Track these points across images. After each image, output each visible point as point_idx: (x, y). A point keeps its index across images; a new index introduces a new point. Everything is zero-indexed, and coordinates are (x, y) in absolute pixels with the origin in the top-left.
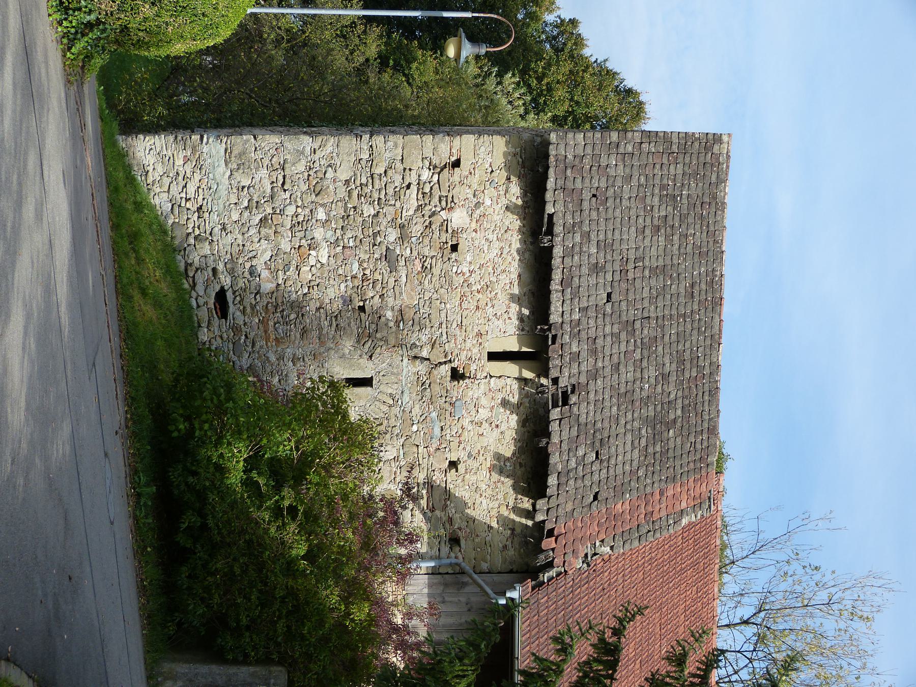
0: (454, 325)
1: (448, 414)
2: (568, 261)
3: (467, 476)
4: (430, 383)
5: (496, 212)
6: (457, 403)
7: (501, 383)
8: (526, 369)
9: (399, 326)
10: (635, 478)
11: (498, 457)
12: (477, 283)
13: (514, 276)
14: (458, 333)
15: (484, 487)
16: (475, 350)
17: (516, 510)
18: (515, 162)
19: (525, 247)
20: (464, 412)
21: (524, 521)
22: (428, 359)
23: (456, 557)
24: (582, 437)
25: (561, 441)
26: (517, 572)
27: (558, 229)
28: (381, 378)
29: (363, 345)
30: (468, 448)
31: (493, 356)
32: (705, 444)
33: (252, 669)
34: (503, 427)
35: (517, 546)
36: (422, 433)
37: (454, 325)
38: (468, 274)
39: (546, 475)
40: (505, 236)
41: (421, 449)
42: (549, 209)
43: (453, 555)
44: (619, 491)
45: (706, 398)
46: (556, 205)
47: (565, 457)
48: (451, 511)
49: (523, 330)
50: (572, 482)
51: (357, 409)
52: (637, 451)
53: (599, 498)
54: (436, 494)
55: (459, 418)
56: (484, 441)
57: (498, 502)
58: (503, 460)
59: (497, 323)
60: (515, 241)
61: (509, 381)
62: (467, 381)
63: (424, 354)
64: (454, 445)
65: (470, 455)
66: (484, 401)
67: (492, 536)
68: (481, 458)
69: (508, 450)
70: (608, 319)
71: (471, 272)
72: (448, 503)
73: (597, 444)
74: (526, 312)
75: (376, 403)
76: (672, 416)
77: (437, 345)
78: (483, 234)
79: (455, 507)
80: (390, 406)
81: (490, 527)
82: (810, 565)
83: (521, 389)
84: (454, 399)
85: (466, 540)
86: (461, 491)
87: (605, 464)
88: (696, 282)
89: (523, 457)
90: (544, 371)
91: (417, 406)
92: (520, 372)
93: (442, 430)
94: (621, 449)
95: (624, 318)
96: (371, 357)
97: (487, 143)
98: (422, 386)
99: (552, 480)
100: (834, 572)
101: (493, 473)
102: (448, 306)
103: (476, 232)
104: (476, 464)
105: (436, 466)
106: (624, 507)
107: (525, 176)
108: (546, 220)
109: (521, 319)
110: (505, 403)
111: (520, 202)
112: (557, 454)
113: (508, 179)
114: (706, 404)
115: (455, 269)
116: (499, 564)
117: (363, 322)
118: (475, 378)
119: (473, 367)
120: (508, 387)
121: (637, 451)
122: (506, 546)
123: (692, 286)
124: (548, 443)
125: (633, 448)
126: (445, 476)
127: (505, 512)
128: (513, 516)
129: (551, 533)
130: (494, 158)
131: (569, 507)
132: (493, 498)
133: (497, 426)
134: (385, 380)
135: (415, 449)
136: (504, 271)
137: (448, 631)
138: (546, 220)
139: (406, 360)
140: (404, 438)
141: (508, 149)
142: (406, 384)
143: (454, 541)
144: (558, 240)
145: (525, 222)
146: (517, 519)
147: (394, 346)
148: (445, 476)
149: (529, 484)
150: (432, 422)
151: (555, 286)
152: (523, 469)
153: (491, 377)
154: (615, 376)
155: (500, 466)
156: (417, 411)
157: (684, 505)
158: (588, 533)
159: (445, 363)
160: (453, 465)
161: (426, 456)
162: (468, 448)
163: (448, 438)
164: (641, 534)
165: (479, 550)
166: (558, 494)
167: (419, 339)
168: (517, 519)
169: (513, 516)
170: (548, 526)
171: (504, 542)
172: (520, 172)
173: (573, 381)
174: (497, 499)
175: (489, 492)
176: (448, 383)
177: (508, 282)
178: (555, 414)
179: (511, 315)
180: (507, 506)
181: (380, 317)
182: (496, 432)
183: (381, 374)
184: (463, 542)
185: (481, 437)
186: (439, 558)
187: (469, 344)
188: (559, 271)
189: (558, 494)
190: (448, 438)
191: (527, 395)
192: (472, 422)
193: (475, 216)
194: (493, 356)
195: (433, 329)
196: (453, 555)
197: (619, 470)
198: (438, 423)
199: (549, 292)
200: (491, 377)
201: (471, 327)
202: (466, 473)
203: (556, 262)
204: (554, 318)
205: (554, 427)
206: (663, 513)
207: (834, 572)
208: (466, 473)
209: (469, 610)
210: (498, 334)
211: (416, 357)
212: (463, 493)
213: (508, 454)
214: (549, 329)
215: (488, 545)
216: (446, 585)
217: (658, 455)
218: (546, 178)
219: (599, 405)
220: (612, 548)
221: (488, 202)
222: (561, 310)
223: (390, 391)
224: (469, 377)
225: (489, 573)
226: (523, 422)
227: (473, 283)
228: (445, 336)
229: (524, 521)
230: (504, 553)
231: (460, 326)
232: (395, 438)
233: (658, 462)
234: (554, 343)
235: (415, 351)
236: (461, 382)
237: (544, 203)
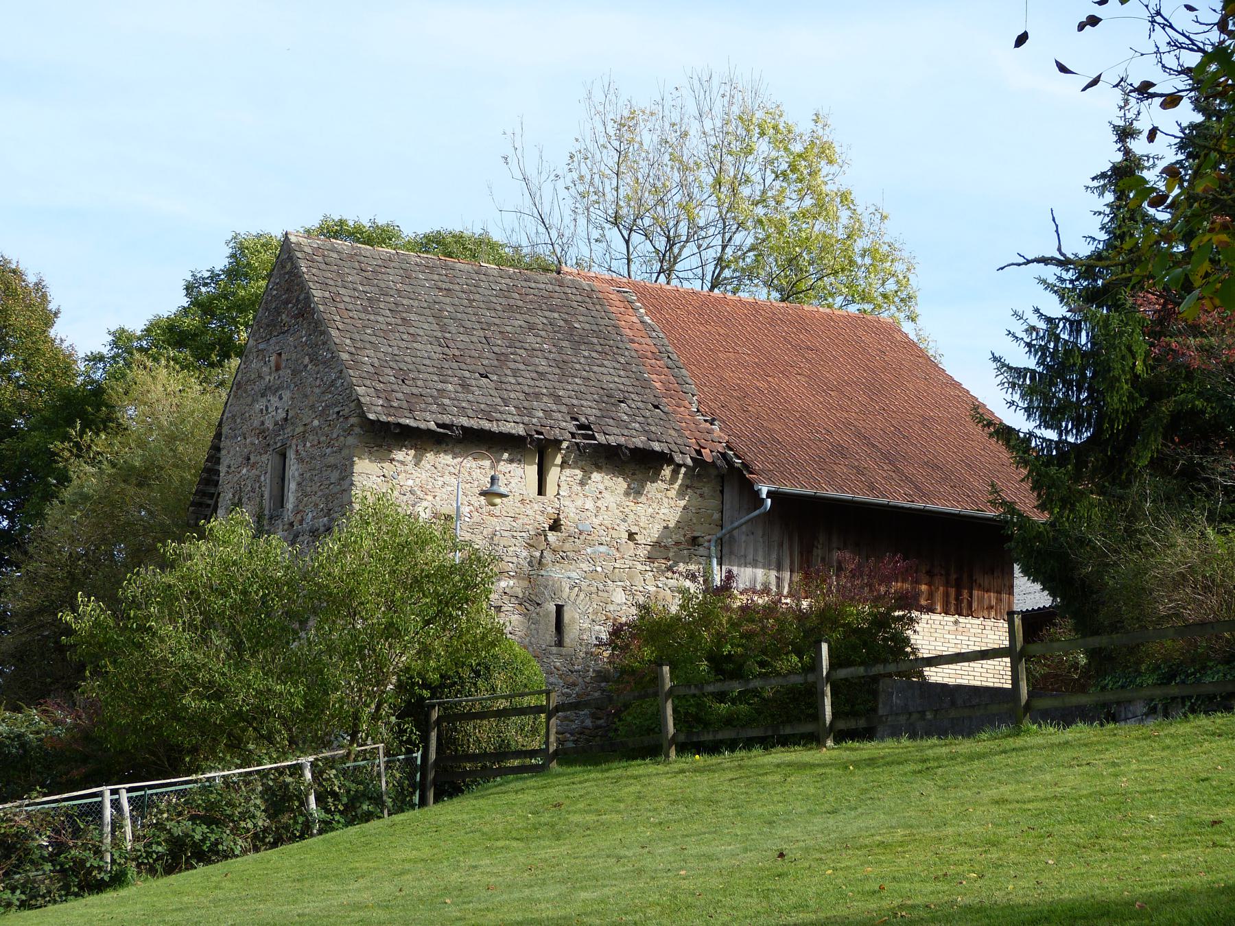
1: (588, 537)
2: (470, 413)
3: (641, 524)
7: (564, 486)
10: (628, 367)
11: (627, 494)
13: (474, 464)
15: (650, 510)
16: (536, 507)
21: (681, 476)
24: (613, 415)
26: (723, 486)
27: (446, 419)
31: (541, 491)
33: (880, 706)
34: (601, 487)
39: (653, 452)
40: (440, 469)
41: (617, 565)
42: (432, 426)
45: (533, 285)
47: (634, 433)
50: (653, 429)
54: (654, 555)
56: (613, 506)
59: (513, 485)
60: (446, 459)
61: (563, 478)
62: (561, 517)
63: (538, 554)
66: (579, 503)
69: (621, 484)
74: (506, 456)
76: (562, 323)
80: (580, 590)
81: (685, 508)
83: (570, 467)
86: (655, 532)
87: (627, 395)
90: (557, 443)
92: (556, 465)
94: (609, 378)
96: (538, 604)
99: (657, 447)
100: (577, 140)
101: (640, 500)
102: (498, 529)
104: (632, 516)
105: (631, 552)
107: (389, 446)
108: (442, 430)
109: (511, 461)
110: (582, 483)
111: (412, 452)
115: (467, 519)
116: (715, 503)
118: (559, 509)
119: (550, 510)
123: (440, 289)
124: (626, 447)
125: (602, 365)
127: (672, 493)
128: (676, 486)
129: (699, 452)
132: (660, 503)
135: (617, 570)
136: (470, 473)
137: (769, 555)
138: (442, 430)
139: (543, 572)
140: (607, 580)
146: (679, 482)
149: (651, 468)
151: (494, 427)
152: (637, 472)
153: (558, 494)
155: (635, 492)
156: (585, 566)
160: (631, 536)
161: (623, 561)
163: (608, 539)
167: (525, 558)
168: (679, 482)
169: (676, 486)
170: (694, 454)
175: (655, 505)
182: (606, 494)
184: (696, 534)
186: (709, 557)
187: (530, 512)
188: (482, 422)
190: (608, 539)
191: (575, 462)
192: (596, 516)
194: (541, 491)
196: (706, 544)
200: (558, 494)
203: (474, 423)
204: (520, 430)
205: (613, 440)
206: (648, 341)
211: (540, 563)
212: (655, 529)
216: (731, 553)
218: (408, 426)
219: (580, 395)
220: (693, 395)
221: (410, 482)
225: (722, 512)
226: (599, 468)
228: (523, 534)
229: (681, 476)
233: (608, 342)
234: (541, 434)
235: (535, 562)
237: (429, 431)
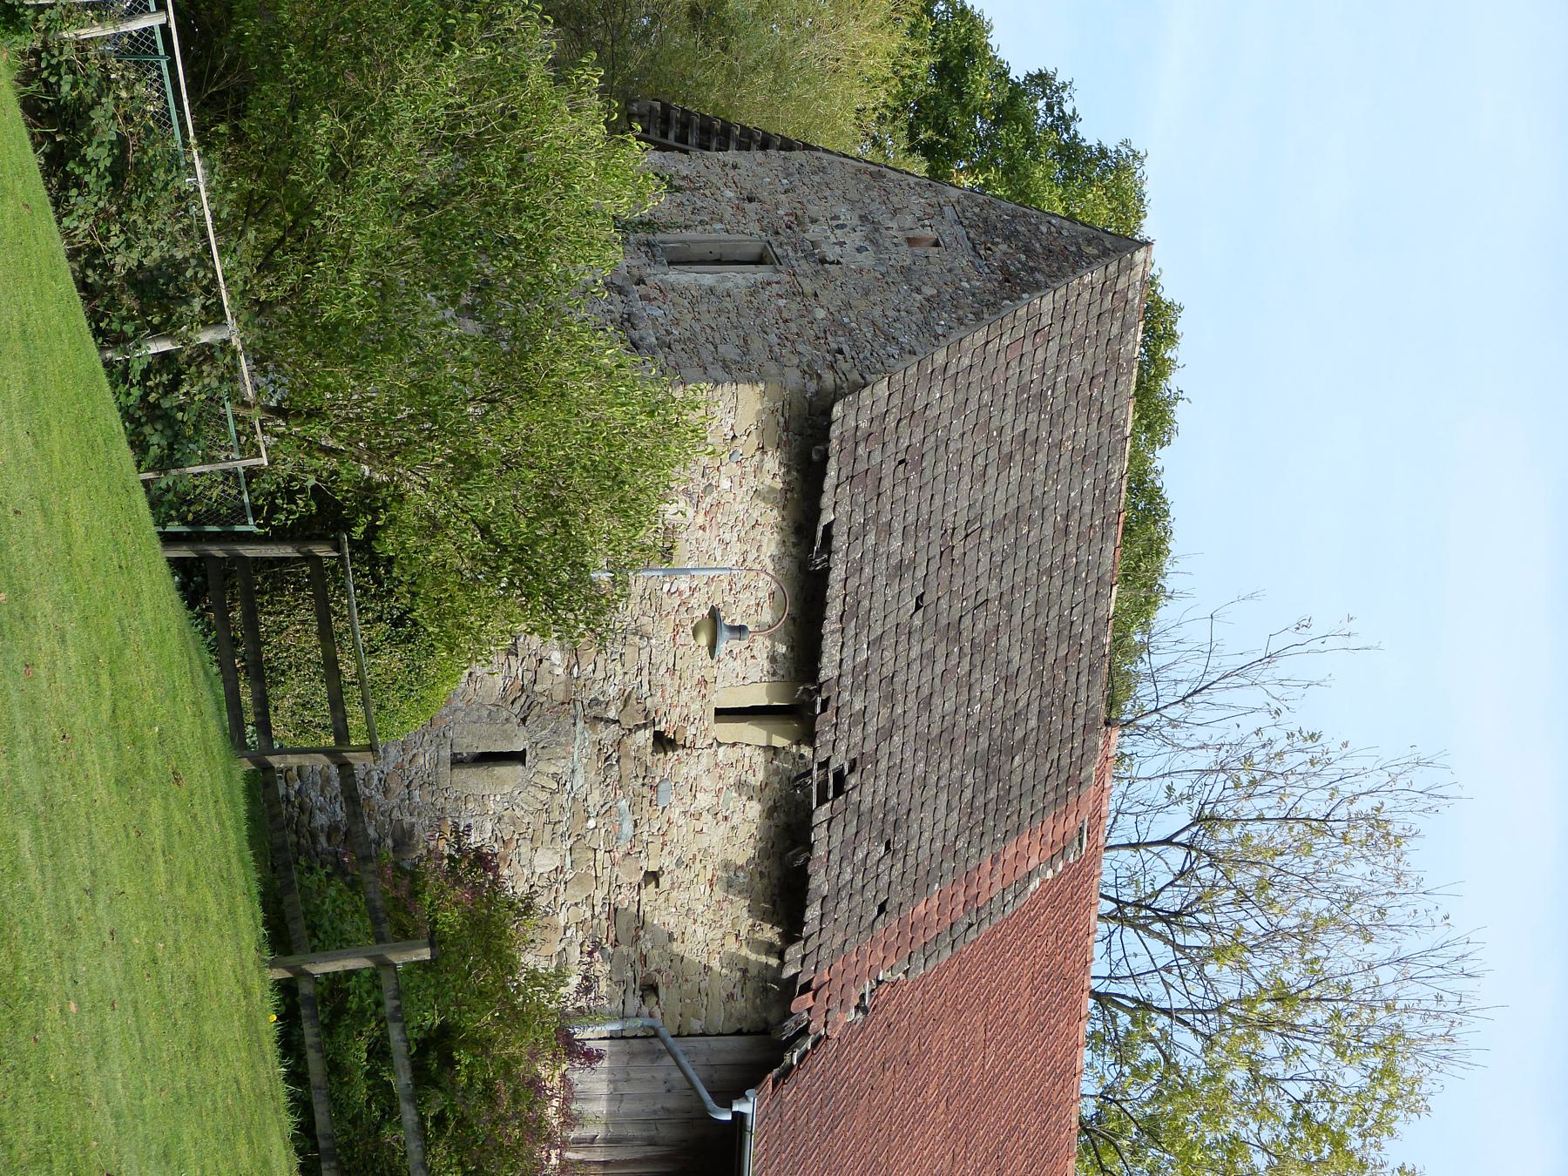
0: (663, 670)
1: (646, 802)
3: (674, 893)
4: (619, 758)
5: (738, 499)
6: (662, 787)
7: (734, 754)
8: (777, 734)
9: (571, 673)
12: (702, 607)
13: (763, 594)
14: (669, 682)
15: (700, 908)
16: (695, 706)
17: (750, 943)
18: (773, 423)
19: (783, 550)
20: (672, 798)
22: (618, 721)
23: (651, 1015)
24: (864, 833)
25: (829, 852)
26: (748, 1033)
27: (839, 542)
28: (539, 751)
29: (512, 703)
30: (677, 852)
31: (722, 714)
32: (1078, 752)
35: (751, 996)
36: (603, 831)
37: (663, 670)
38: (688, 594)
39: (802, 907)
40: (752, 534)
41: (600, 855)
42: (827, 517)
43: (645, 1010)
44: (919, 888)
45: (1084, 680)
46: (838, 508)
48: (646, 945)
49: (774, 674)
51: (498, 798)
52: (955, 814)
53: (888, 908)
55: (664, 808)
56: (704, 841)
57: (722, 930)
58: (733, 868)
59: (732, 664)
60: (770, 544)
62: (680, 752)
63: (612, 714)
64: (654, 848)
65: (679, 863)
66: (706, 782)
67: (711, 980)
68: (698, 866)
69: (743, 851)
70: (916, 637)
71: (693, 590)
72: (642, 933)
73: (889, 831)
75: (529, 788)
77: (633, 701)
78: (715, 533)
79: (653, 940)
81: (707, 968)
82: (1300, 732)
84: (657, 780)
85: (668, 987)
86: (662, 916)
87: (901, 855)
88: (1084, 408)
89: (766, 863)
90: (809, 737)
91: (596, 793)
92: (769, 738)
93: (636, 826)
95: (943, 622)
96: (524, 720)
97: (728, 396)
98: (606, 760)
99: (812, 913)
102: (653, 641)
103: (704, 530)
105: (624, 879)
106: (929, 905)
107: (788, 443)
108: (820, 534)
109: (773, 659)
110: (740, 785)
112: (823, 871)
113: (762, 449)
114: (1083, 689)
116: (719, 1021)
117: (513, 669)
118: (692, 747)
119: (690, 731)
120: (747, 760)
121: (955, 814)
122: (732, 995)
123: (1067, 517)
124: (808, 860)
126: (639, 893)
128: (745, 951)
129: (806, 988)
130: (738, 418)
131: (838, 940)
133: (726, 818)
134: (546, 754)
135: (591, 854)
136: (747, 587)
137: (634, 1122)
138: (820, 534)
141: (762, 404)
142: (580, 760)
143: (650, 989)
144: (837, 559)
145: (784, 513)
146: (753, 957)
147: (563, 704)
148: (639, 893)
150: (620, 815)
151: (830, 626)
152: (765, 881)
153: (720, 744)
154: (924, 718)
156: (595, 798)
157: (1034, 861)
158: (868, 965)
159: (645, 726)
160: (653, 877)
161: (608, 864)
162: (677, 852)
163: (645, 837)
164: (955, 936)
165: (688, 1001)
166: (821, 930)
167: (603, 693)
168: (753, 957)
169: (745, 951)
171: (730, 990)
172: (780, 438)
173: (852, 755)
174: (721, 926)
176: (649, 756)
177: (753, 602)
178: (821, 814)
179: (755, 653)
180: (737, 936)
181: (541, 661)
182: (724, 828)
183: (540, 746)
184: (662, 991)
185: (698, 836)
186: (623, 1017)
188: (839, 601)
189: (821, 930)
191: (777, 772)
192: (685, 813)
193: (704, 505)
194: (722, 714)
195: (627, 677)
196: (645, 1010)
197: (924, 854)
198: (630, 816)
199: (820, 638)
200: (720, 744)
201: (689, 672)
202: (672, 888)
203: (835, 590)
204: (827, 671)
205: (819, 834)
207: (1345, 745)
208: (672, 888)
209: (669, 1091)
210: (734, 682)
213: (741, 861)
214: (819, 691)
215: (703, 994)
216: (632, 1055)
217: (991, 806)
218: (823, 474)
220: (906, 972)
221: (726, 484)
222: (838, 658)
223: (552, 770)
224: (684, 746)
225: (703, 1035)
227: (696, 606)
228: (646, 687)
230: (728, 1006)
231: (672, 670)
232: (559, 840)
235: (597, 710)
236: (670, 754)
237: (818, 512)
